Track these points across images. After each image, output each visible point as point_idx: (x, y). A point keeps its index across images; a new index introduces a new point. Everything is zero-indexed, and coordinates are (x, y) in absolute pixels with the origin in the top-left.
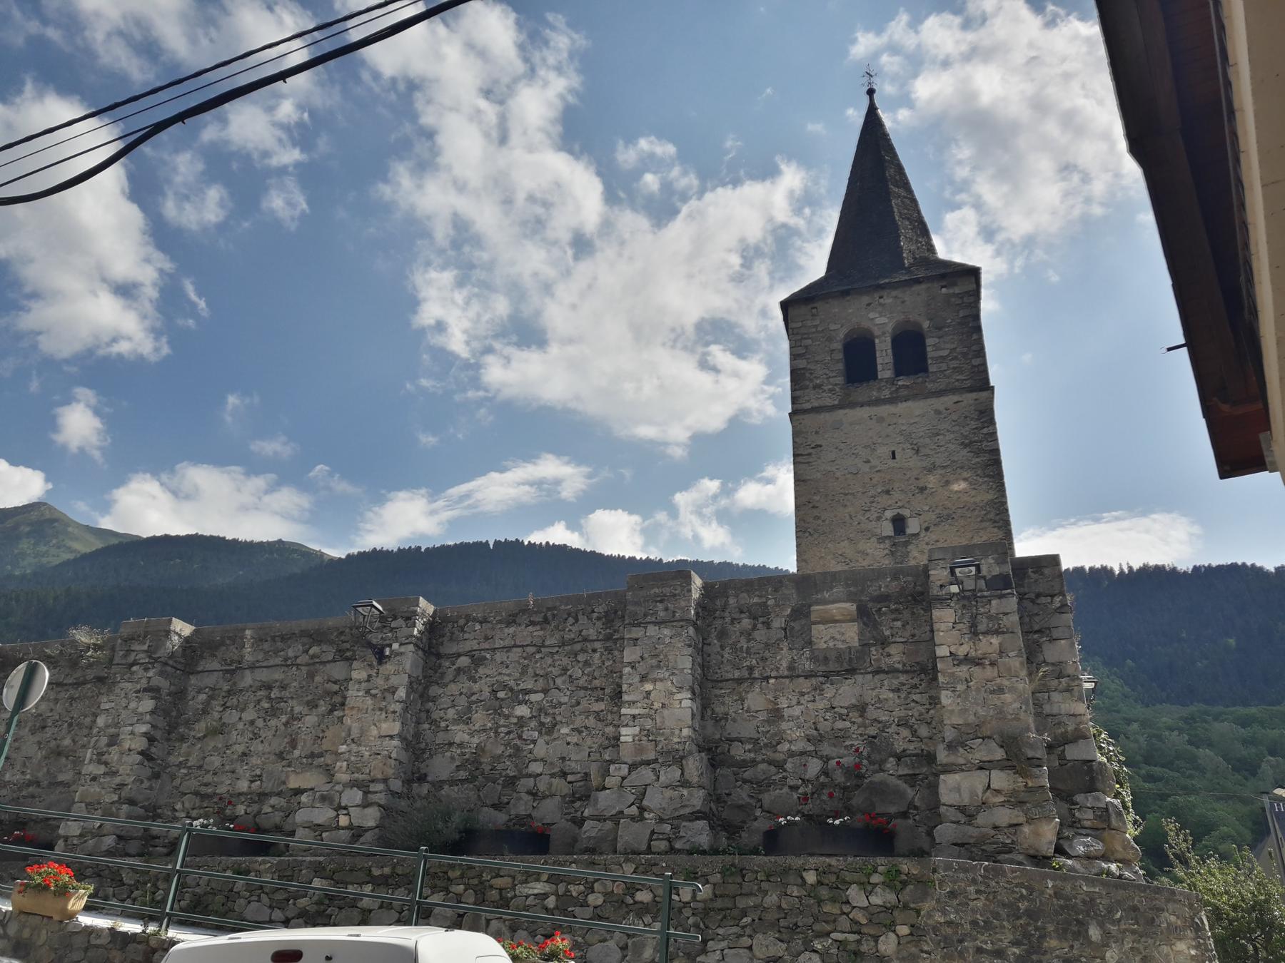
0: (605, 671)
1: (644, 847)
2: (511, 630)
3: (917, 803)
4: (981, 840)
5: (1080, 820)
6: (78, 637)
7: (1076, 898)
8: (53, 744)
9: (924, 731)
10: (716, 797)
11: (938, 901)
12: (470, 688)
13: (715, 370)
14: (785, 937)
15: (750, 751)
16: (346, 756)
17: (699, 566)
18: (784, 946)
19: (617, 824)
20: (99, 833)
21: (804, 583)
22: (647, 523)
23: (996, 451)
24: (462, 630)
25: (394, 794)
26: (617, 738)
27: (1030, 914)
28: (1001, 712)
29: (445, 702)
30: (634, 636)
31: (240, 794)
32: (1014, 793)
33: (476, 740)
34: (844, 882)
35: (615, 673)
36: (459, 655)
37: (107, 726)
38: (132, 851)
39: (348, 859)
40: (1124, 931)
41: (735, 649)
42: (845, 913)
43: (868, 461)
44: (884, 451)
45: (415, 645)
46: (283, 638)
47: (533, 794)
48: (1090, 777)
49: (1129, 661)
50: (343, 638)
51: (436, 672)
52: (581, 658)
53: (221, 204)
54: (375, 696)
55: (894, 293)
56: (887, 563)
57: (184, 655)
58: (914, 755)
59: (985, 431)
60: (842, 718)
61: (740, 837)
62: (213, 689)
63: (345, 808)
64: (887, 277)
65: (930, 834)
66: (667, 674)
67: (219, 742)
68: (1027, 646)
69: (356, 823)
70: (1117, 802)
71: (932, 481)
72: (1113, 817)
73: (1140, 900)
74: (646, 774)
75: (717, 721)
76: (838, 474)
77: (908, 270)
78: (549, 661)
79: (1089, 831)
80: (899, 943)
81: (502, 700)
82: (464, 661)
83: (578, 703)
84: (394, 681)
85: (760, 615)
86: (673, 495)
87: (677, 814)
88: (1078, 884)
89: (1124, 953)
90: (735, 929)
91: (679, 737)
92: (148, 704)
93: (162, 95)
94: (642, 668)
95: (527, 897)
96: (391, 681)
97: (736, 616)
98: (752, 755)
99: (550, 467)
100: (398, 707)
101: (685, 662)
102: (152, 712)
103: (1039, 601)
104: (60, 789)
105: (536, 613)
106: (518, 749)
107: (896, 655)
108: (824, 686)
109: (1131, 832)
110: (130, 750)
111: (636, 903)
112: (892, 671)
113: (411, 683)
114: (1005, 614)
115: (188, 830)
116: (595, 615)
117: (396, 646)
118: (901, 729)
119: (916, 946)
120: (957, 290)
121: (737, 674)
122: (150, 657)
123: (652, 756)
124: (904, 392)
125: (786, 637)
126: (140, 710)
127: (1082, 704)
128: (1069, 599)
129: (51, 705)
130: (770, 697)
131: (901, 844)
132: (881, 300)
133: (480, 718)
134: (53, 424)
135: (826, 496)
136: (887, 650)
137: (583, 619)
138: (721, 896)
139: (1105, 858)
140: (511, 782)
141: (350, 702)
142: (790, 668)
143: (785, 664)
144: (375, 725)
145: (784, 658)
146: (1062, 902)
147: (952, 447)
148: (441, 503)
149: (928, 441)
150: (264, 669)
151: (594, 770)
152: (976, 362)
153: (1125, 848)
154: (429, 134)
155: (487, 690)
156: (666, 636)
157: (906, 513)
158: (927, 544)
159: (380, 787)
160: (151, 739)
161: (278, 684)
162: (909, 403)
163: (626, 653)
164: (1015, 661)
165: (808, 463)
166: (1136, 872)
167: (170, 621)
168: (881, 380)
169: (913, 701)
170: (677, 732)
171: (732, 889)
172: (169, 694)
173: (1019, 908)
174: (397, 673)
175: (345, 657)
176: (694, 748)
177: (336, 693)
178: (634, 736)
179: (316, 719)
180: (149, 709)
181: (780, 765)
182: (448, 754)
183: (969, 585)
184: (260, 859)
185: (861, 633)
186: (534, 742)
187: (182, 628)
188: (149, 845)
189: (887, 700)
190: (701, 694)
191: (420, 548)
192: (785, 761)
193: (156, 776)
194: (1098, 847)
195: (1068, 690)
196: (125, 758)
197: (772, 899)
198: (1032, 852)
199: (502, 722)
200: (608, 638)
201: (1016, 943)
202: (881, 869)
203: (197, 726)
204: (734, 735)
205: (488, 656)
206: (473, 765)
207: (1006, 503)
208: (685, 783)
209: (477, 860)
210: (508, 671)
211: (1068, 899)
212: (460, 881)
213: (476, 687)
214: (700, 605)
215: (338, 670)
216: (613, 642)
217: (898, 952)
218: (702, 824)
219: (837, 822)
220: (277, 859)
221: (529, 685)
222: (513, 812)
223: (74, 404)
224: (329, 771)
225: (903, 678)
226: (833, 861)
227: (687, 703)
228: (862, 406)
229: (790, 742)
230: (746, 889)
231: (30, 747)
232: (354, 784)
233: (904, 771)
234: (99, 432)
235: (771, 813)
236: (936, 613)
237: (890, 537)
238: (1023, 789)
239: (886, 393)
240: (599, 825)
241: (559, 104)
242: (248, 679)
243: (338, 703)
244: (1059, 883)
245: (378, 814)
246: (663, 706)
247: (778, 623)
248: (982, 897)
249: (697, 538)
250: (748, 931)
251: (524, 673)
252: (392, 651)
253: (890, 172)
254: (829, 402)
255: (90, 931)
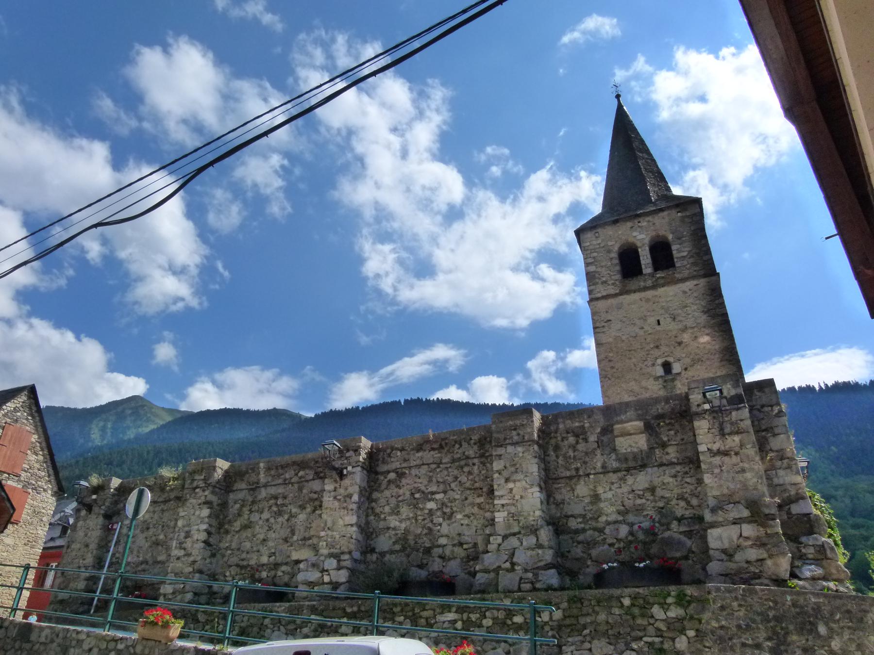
0: (482, 477)
1: (516, 588)
2: (420, 454)
3: (694, 549)
4: (739, 571)
5: (805, 554)
6: (163, 474)
7: (807, 607)
8: (154, 538)
9: (695, 502)
10: (560, 553)
11: (713, 613)
12: (397, 493)
13: (543, 280)
14: (613, 641)
15: (580, 523)
16: (325, 538)
17: (538, 406)
18: (612, 647)
19: (498, 574)
20: (183, 591)
21: (610, 411)
22: (511, 382)
23: (725, 315)
24: (389, 455)
25: (356, 561)
26: (493, 520)
27: (777, 619)
28: (745, 485)
29: (382, 501)
30: (499, 453)
31: (263, 565)
32: (758, 538)
33: (403, 526)
34: (648, 603)
35: (489, 478)
36: (388, 472)
37: (184, 526)
38: (202, 601)
39: (331, 603)
40: (842, 628)
41: (566, 457)
42: (651, 624)
43: (642, 328)
44: (652, 320)
45: (362, 467)
46: (282, 467)
47: (442, 557)
48: (809, 525)
49: (833, 448)
50: (318, 465)
51: (375, 483)
52: (466, 469)
53: (239, 213)
54: (339, 500)
55: (647, 219)
56: (662, 393)
57: (225, 481)
58: (691, 518)
59: (717, 302)
60: (640, 497)
61: (579, 579)
62: (243, 501)
63: (327, 571)
64: (641, 209)
65: (704, 569)
66: (522, 477)
67: (248, 533)
68: (758, 440)
69: (334, 580)
70: (830, 541)
71: (686, 337)
72: (828, 552)
73: (853, 606)
74: (514, 542)
75: (557, 505)
76: (624, 338)
77: (654, 204)
78: (446, 473)
79: (812, 561)
80: (689, 642)
81: (418, 499)
82: (392, 476)
83: (466, 499)
84: (350, 490)
85: (580, 434)
86: (526, 363)
87: (536, 566)
88: (808, 597)
89: (844, 642)
90: (580, 638)
91: (534, 517)
92: (206, 512)
93: (200, 153)
94: (506, 474)
95: (444, 622)
96: (349, 490)
97: (564, 435)
98: (582, 525)
99: (441, 352)
100: (354, 506)
101: (533, 468)
102: (209, 517)
103: (763, 410)
104: (160, 565)
105: (434, 442)
106: (430, 529)
107: (672, 453)
108: (627, 477)
109: (842, 560)
110: (197, 540)
111: (514, 623)
112: (671, 464)
113: (361, 491)
114: (741, 420)
115: (235, 586)
116: (472, 442)
117: (350, 468)
118: (680, 502)
119: (700, 644)
120: (688, 214)
121: (568, 474)
122: (205, 483)
123: (516, 530)
124: (661, 281)
125: (599, 447)
126: (202, 515)
127: (799, 476)
128: (784, 407)
129: (151, 515)
130: (591, 487)
131: (685, 577)
132: (640, 224)
133: (405, 511)
134: (151, 354)
135: (617, 352)
136: (666, 450)
137: (465, 445)
138: (569, 617)
139: (825, 578)
140: (428, 551)
141: (325, 504)
142: (603, 467)
143: (599, 465)
144: (341, 518)
145: (598, 461)
146: (798, 610)
147: (696, 314)
148: (376, 379)
149: (680, 311)
150: (273, 487)
151: (480, 540)
152: (705, 258)
153: (838, 571)
154: (361, 160)
155: (408, 493)
156: (519, 452)
157: (671, 359)
158: (687, 379)
159: (346, 557)
160: (209, 533)
161: (281, 495)
162: (665, 288)
163: (495, 464)
164: (751, 451)
165: (603, 332)
166: (847, 587)
167: (215, 461)
168: (645, 275)
169: (686, 482)
170: (532, 513)
171: (575, 611)
172: (218, 505)
173: (768, 615)
174: (352, 485)
175: (320, 476)
176: (544, 523)
177: (316, 499)
178: (504, 518)
179: (305, 516)
180: (207, 515)
181: (601, 531)
182: (387, 535)
183: (716, 403)
184: (278, 604)
185: (648, 441)
186: (440, 525)
187: (223, 465)
188: (212, 596)
189: (668, 483)
190: (546, 488)
191: (358, 407)
192: (604, 528)
193: (213, 555)
194: (819, 572)
195: (789, 467)
196: (195, 545)
197: (602, 617)
198: (774, 577)
199: (419, 513)
200: (482, 456)
201: (769, 639)
202: (673, 593)
203: (235, 524)
204: (570, 513)
205: (407, 472)
206: (404, 543)
207: (735, 348)
208: (540, 546)
209: (409, 599)
210: (420, 481)
211: (802, 607)
212: (400, 614)
213: (401, 492)
214: (540, 430)
215: (316, 485)
216: (485, 458)
217: (689, 648)
218: (553, 571)
219: (642, 565)
220: (288, 604)
221: (434, 488)
222: (431, 570)
223: (162, 344)
224: (315, 549)
225: (678, 468)
226: (641, 590)
227: (538, 494)
228: (635, 292)
229: (607, 515)
230: (584, 612)
231: (141, 541)
232: (331, 555)
233: (682, 529)
234: (176, 357)
235: (598, 562)
236: (696, 424)
237: (661, 377)
238: (764, 535)
239: (649, 283)
240: (486, 575)
241: (436, 130)
242: (263, 493)
243: (317, 505)
244: (794, 597)
245: (347, 574)
246: (522, 497)
247: (593, 438)
248: (743, 609)
249: (544, 391)
250: (588, 638)
251: (430, 481)
252: (348, 472)
253: (636, 144)
254: (612, 292)
255: (183, 650)
